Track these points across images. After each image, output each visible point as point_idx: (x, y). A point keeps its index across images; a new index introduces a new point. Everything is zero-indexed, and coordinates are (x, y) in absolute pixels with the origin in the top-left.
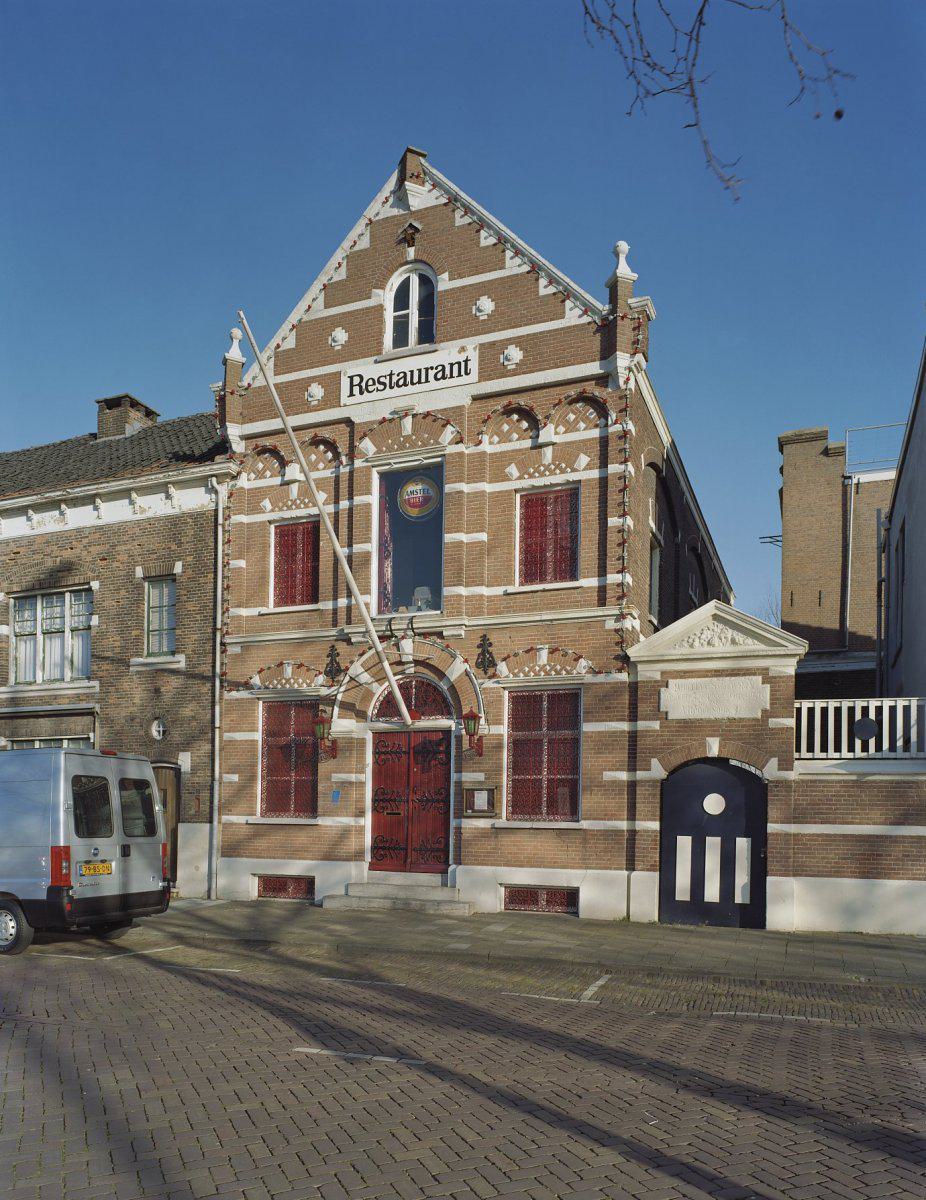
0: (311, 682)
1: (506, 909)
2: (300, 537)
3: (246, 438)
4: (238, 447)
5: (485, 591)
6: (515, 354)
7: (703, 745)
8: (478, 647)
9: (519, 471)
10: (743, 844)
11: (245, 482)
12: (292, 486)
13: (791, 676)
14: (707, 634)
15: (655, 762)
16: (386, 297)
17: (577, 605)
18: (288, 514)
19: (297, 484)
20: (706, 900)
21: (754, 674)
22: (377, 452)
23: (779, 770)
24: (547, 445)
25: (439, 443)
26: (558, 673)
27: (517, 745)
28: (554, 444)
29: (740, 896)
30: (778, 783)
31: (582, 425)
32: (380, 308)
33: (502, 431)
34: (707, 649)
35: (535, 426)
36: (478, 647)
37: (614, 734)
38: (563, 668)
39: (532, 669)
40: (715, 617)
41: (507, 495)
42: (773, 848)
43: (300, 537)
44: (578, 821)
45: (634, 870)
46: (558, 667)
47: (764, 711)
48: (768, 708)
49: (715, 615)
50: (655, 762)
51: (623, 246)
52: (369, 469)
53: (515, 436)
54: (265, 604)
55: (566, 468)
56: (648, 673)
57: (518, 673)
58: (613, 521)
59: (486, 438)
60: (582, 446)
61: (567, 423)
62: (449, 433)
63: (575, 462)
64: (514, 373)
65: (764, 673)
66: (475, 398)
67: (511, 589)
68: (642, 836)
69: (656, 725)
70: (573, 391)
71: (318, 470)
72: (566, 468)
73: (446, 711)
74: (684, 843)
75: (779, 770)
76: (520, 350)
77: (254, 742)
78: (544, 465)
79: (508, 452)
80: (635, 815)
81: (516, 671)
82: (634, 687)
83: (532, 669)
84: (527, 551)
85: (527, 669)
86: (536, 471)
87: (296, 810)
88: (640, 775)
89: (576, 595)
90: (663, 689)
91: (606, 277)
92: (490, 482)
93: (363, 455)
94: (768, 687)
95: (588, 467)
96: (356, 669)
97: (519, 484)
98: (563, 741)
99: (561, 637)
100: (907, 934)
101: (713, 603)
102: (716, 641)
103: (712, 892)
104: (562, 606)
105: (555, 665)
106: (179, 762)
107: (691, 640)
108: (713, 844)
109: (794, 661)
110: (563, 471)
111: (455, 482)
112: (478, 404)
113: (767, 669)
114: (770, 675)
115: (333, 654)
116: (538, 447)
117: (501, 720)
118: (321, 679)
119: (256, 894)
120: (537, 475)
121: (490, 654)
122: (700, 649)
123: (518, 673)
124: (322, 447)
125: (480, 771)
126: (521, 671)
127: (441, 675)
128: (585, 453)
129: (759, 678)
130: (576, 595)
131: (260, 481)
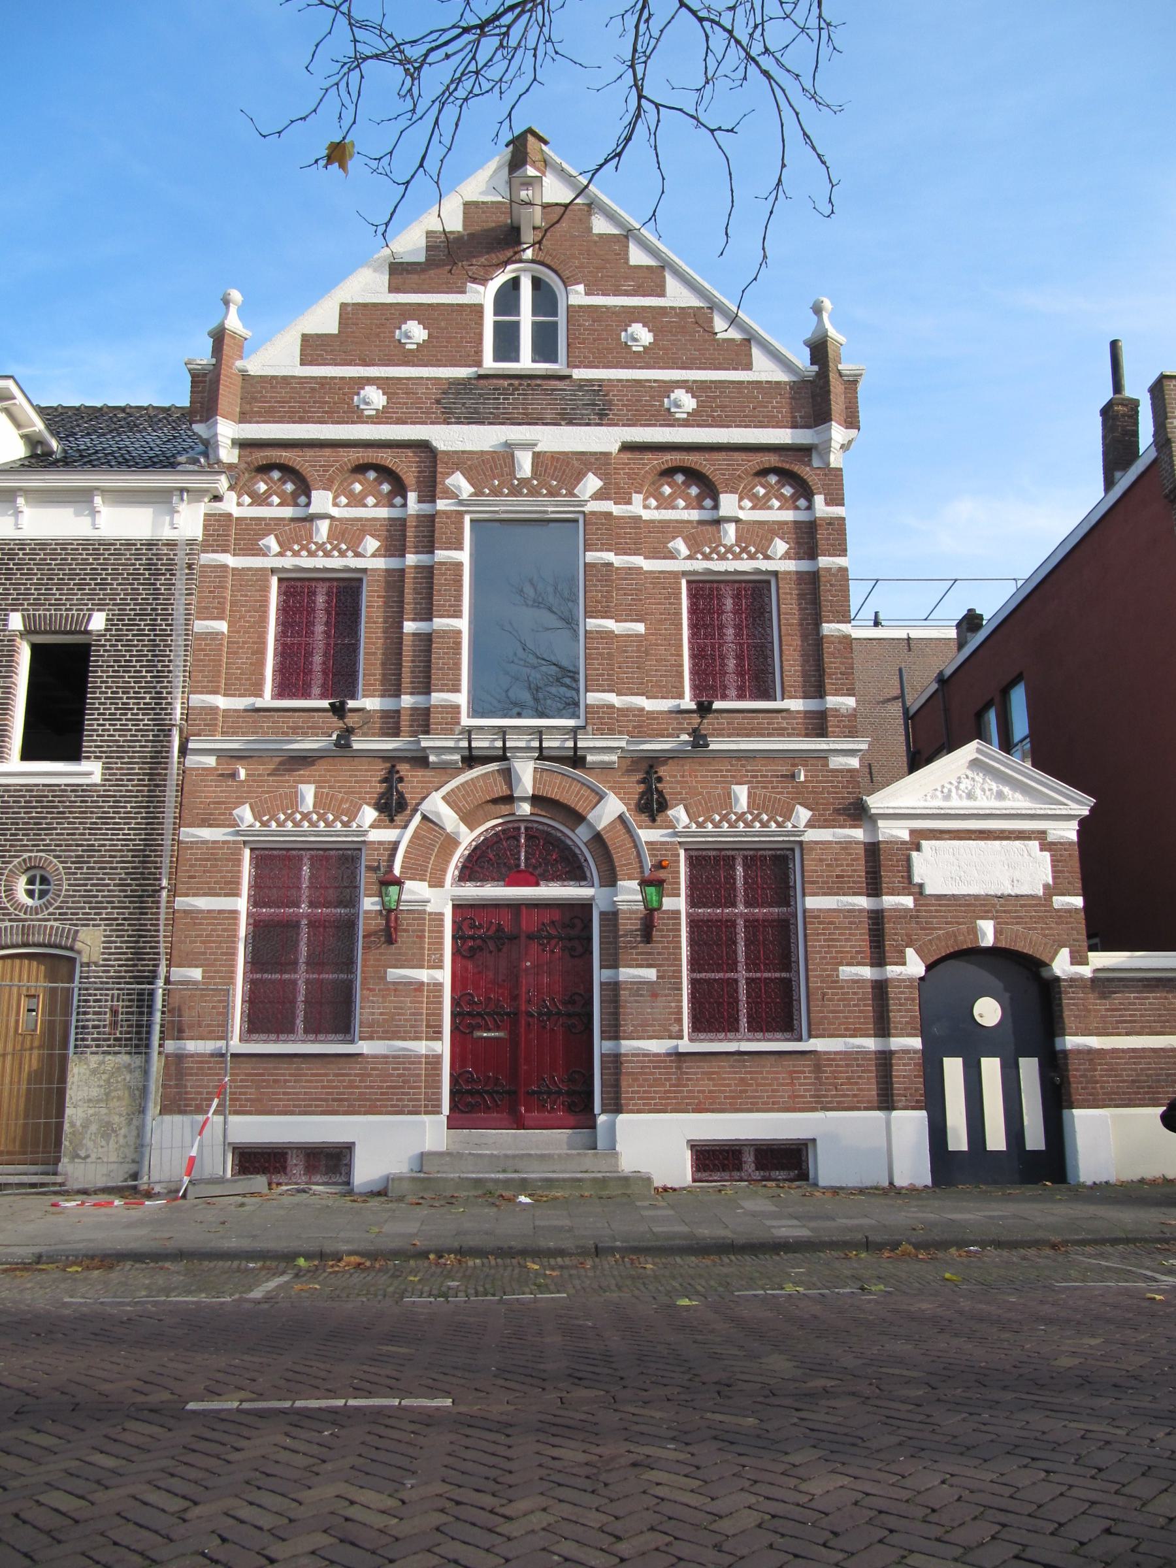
0: (349, 822)
1: (694, 1181)
2: (321, 600)
3: (244, 445)
4: (228, 454)
5: (221, 702)
6: (376, 398)
7: (974, 931)
8: (381, 782)
9: (689, 549)
10: (1029, 1068)
11: (231, 505)
12: (319, 522)
13: (1071, 843)
14: (966, 784)
15: (910, 953)
16: (485, 295)
17: (781, 732)
18: (306, 562)
19: (327, 522)
20: (1044, 1148)
21: (1029, 839)
22: (475, 494)
23: (1072, 964)
24: (728, 520)
25: (575, 496)
26: (764, 825)
27: (261, 930)
28: (332, 518)
29: (1035, 1139)
30: (1074, 981)
31: (681, 503)
32: (478, 309)
33: (661, 494)
34: (966, 803)
35: (304, 488)
36: (381, 782)
37: (850, 912)
38: (336, 819)
39: (724, 818)
40: (975, 764)
41: (262, 575)
42: (1076, 1070)
43: (321, 600)
44: (352, 1042)
45: (894, 1108)
46: (331, 817)
47: (1046, 886)
48: (1051, 882)
49: (976, 760)
50: (910, 953)
51: (236, 295)
52: (461, 514)
53: (276, 500)
54: (259, 694)
55: (756, 553)
56: (895, 831)
57: (705, 821)
58: (409, 627)
59: (637, 498)
60: (775, 529)
61: (754, 497)
62: (592, 483)
63: (769, 547)
64: (685, 423)
65: (1041, 835)
66: (627, 447)
67: (259, 703)
68: (900, 1058)
69: (908, 901)
70: (772, 460)
71: (365, 506)
72: (756, 553)
73: (577, 874)
74: (953, 1068)
75: (1072, 964)
76: (384, 394)
77: (234, 914)
78: (724, 546)
79: (670, 521)
80: (617, 1026)
81: (701, 819)
82: (873, 850)
83: (289, 817)
84: (285, 652)
85: (717, 818)
86: (713, 551)
87: (306, 1031)
88: (892, 971)
89: (779, 720)
90: (914, 854)
91: (213, 324)
92: (234, 555)
93: (450, 494)
94: (1047, 855)
95: (786, 556)
96: (437, 805)
97: (689, 566)
98: (766, 922)
99: (766, 776)
100: (1113, 1180)
101: (974, 744)
102: (978, 792)
103: (996, 1139)
104: (748, 733)
105: (759, 814)
106: (78, 945)
107: (945, 790)
108: (991, 1067)
109: (1074, 825)
110: (752, 557)
111: (601, 550)
112: (626, 456)
113: (1044, 832)
114: (1049, 840)
115: (391, 778)
116: (311, 518)
117: (238, 889)
118: (369, 814)
119: (689, 1178)
120: (715, 556)
121: (661, 793)
122: (958, 803)
123: (705, 821)
124: (680, 478)
125: (650, 966)
126: (273, 817)
127: (577, 818)
128: (782, 538)
129: (1036, 843)
130: (779, 720)
131: (663, 511)
